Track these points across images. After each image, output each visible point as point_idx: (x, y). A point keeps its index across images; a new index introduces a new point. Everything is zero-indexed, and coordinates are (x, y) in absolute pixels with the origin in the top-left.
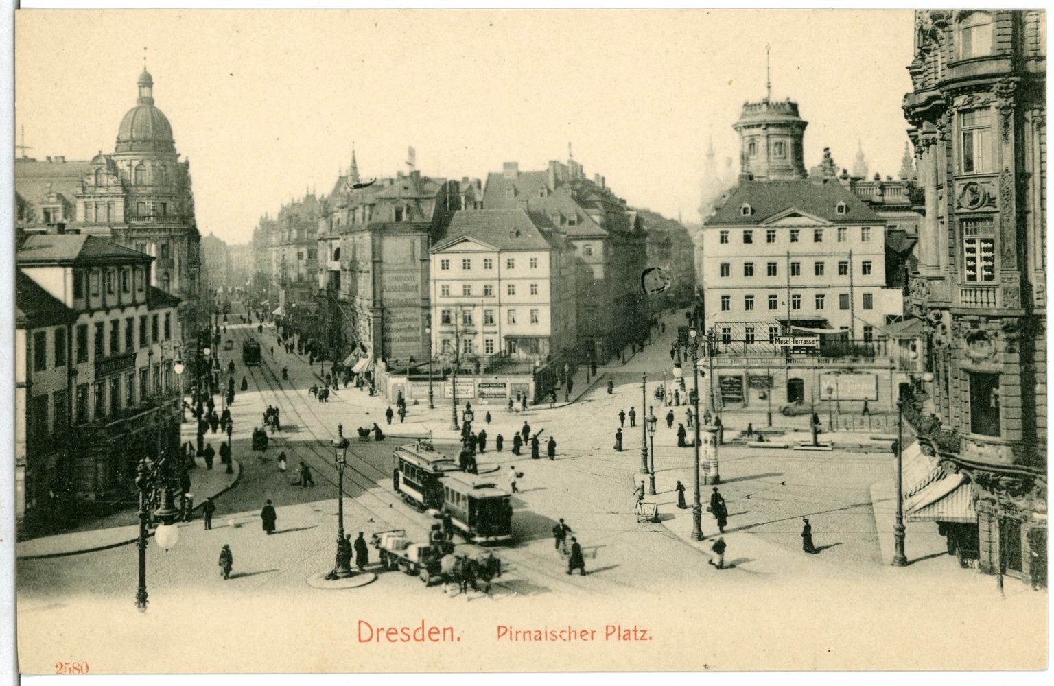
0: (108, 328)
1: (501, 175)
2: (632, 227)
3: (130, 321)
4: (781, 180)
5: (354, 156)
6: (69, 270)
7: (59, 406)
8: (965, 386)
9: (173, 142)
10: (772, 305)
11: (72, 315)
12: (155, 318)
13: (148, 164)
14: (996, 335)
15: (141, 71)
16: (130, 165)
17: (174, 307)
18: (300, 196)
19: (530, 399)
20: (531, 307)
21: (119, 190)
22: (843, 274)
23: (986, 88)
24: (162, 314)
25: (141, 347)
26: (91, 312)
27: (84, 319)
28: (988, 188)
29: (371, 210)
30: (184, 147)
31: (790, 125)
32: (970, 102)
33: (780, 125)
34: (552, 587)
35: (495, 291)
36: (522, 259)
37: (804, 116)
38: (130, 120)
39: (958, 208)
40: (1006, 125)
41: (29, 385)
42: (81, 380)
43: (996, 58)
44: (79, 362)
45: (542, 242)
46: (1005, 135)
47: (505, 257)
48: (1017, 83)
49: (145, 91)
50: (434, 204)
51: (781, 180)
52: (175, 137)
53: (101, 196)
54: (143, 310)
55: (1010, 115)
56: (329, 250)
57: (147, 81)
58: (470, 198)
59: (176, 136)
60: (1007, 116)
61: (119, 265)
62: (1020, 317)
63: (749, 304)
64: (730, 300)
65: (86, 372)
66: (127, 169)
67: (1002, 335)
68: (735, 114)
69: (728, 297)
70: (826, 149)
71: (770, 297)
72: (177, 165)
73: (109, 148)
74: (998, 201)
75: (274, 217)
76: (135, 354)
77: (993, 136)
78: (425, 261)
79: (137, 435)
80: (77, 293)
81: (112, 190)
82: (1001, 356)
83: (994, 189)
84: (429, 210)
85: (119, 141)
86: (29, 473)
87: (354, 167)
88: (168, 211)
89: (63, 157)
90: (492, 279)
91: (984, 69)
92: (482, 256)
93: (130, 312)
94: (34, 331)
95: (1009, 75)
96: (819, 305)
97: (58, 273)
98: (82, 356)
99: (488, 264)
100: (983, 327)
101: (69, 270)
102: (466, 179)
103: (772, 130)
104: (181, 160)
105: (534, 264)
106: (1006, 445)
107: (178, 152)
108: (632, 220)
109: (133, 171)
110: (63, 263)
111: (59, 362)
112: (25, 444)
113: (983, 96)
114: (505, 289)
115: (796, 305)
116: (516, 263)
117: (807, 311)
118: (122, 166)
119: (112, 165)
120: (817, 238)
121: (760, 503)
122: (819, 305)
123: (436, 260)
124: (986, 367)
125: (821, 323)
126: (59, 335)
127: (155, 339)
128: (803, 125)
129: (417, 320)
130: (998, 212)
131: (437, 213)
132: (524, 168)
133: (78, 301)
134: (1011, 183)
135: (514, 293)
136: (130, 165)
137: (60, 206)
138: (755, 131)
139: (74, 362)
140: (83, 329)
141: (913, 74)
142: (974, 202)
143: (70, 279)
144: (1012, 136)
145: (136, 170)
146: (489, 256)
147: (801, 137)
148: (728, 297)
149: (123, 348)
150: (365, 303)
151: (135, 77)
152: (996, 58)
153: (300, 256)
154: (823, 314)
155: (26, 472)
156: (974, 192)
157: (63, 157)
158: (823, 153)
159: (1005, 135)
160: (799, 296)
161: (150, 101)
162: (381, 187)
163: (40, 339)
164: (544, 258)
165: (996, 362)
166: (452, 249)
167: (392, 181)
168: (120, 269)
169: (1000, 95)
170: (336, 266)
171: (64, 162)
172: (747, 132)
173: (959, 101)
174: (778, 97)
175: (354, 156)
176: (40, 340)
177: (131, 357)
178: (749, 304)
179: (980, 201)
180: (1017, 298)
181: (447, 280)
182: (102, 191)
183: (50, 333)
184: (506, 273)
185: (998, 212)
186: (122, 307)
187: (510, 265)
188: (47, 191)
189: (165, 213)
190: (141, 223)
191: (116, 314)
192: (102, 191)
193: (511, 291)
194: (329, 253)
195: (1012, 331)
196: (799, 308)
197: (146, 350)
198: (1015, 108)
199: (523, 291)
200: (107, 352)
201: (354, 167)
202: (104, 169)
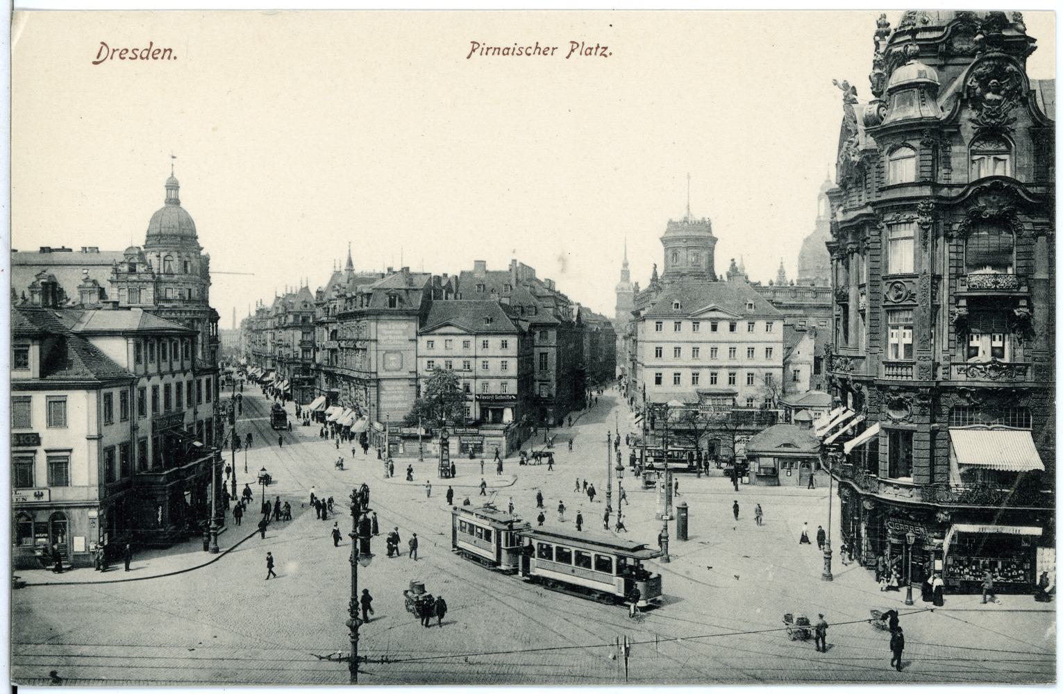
1: (470, 274)
2: (575, 319)
7: (124, 457)
8: (885, 441)
9: (196, 238)
10: (695, 379)
11: (132, 382)
12: (199, 382)
14: (912, 401)
16: (159, 256)
17: (213, 374)
19: (503, 453)
25: (189, 407)
27: (143, 382)
29: (368, 299)
30: (207, 242)
36: (495, 341)
37: (715, 234)
39: (885, 302)
40: (926, 237)
46: (925, 244)
48: (935, 204)
50: (421, 295)
51: (691, 279)
55: (929, 229)
56: (326, 333)
57: (173, 186)
58: (449, 290)
60: (927, 230)
63: (677, 380)
64: (681, 376)
69: (679, 374)
70: (733, 260)
71: (675, 374)
72: (200, 257)
73: (140, 241)
74: (917, 297)
79: (190, 482)
87: (350, 263)
88: (192, 295)
89: (97, 248)
91: (909, 193)
96: (732, 381)
98: (142, 412)
102: (445, 275)
105: (504, 345)
106: (917, 487)
107: (201, 245)
108: (575, 313)
109: (162, 261)
110: (125, 334)
111: (124, 418)
112: (97, 488)
115: (714, 381)
117: (723, 384)
120: (732, 328)
122: (732, 381)
124: (903, 425)
125: (732, 395)
127: (199, 400)
128: (715, 240)
130: (917, 305)
132: (491, 267)
136: (159, 256)
138: (677, 244)
140: (143, 390)
143: (131, 347)
144: (929, 245)
145: (165, 260)
147: (713, 249)
148: (679, 374)
151: (163, 180)
154: (735, 388)
155: (98, 512)
157: (97, 248)
158: (731, 262)
159: (925, 244)
161: (177, 202)
162: (374, 280)
163: (108, 398)
165: (911, 422)
166: (437, 331)
167: (383, 276)
168: (171, 341)
169: (921, 213)
171: (98, 252)
173: (888, 218)
178: (677, 380)
179: (903, 296)
182: (134, 278)
183: (116, 393)
187: (485, 345)
188: (85, 277)
191: (169, 379)
195: (925, 399)
196: (715, 383)
198: (933, 224)
200: (162, 410)
201: (350, 263)
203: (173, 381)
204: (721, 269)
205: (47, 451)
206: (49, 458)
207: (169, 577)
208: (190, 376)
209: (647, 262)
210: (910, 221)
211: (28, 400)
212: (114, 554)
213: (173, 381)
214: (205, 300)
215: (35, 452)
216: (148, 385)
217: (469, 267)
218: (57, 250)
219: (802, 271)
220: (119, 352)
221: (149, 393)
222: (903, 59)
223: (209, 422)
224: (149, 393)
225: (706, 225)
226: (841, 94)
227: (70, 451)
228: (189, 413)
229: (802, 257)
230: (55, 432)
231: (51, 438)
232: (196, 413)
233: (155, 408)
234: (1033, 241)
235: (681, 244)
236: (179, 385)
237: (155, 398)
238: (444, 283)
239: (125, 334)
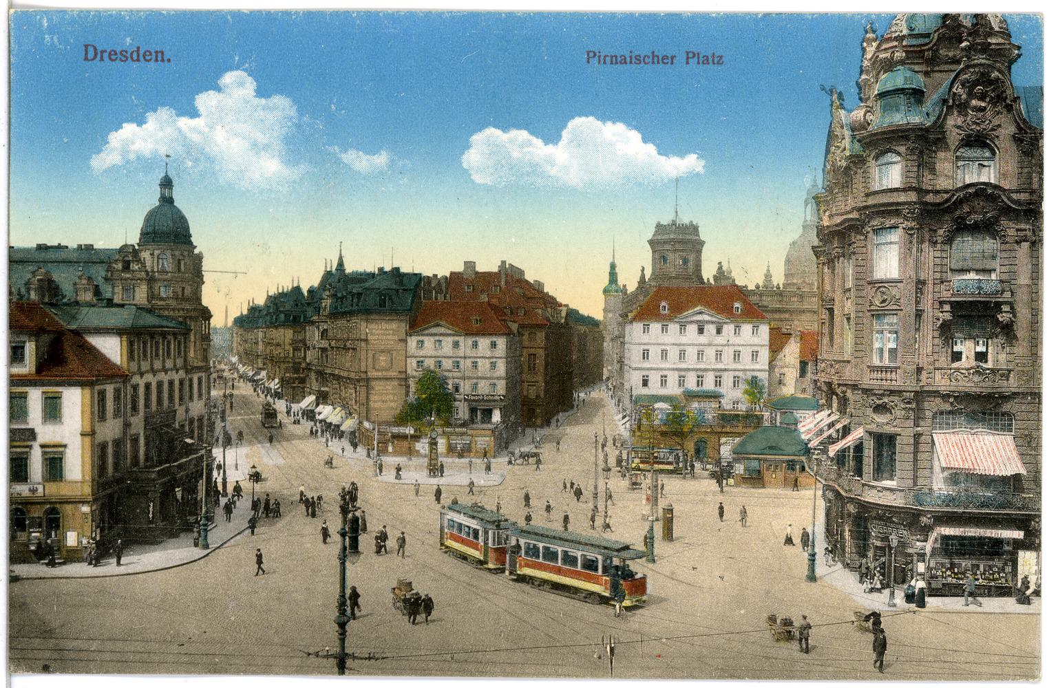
0: (166, 387)
3: (171, 383)
5: (341, 254)
9: (190, 236)
12: (191, 380)
15: (163, 175)
18: (287, 285)
22: (729, 357)
25: (180, 405)
36: (484, 342)
38: (151, 217)
42: (133, 431)
43: (904, 190)
44: (132, 415)
52: (192, 231)
54: (182, 373)
59: (193, 230)
61: (164, 335)
62: (916, 392)
76: (175, 411)
80: (131, 356)
86: (94, 508)
88: (186, 294)
90: (461, 357)
92: (450, 339)
93: (162, 376)
94: (97, 388)
95: (915, 203)
99: (456, 345)
102: (435, 276)
104: (196, 251)
105: (494, 345)
108: (564, 314)
109: (156, 259)
117: (709, 385)
120: (719, 331)
121: (153, 489)
124: (889, 429)
125: (715, 396)
126: (117, 391)
127: (191, 398)
129: (881, 361)
130: (901, 310)
133: (132, 364)
139: (129, 415)
140: (135, 387)
145: (158, 258)
146: (456, 338)
152: (904, 190)
160: (666, 377)
163: (102, 394)
164: (501, 342)
166: (426, 332)
173: (876, 222)
175: (341, 254)
181: (422, 357)
183: (110, 389)
185: (901, 310)
186: (154, 372)
189: (183, 295)
190: (162, 303)
194: (317, 334)
197: (184, 408)
198: (918, 229)
199: (484, 366)
204: (708, 273)
205: (42, 446)
206: (44, 453)
214: (197, 298)
216: (141, 382)
217: (460, 268)
221: (141, 391)
224: (141, 391)
232: (187, 411)
233: (147, 406)
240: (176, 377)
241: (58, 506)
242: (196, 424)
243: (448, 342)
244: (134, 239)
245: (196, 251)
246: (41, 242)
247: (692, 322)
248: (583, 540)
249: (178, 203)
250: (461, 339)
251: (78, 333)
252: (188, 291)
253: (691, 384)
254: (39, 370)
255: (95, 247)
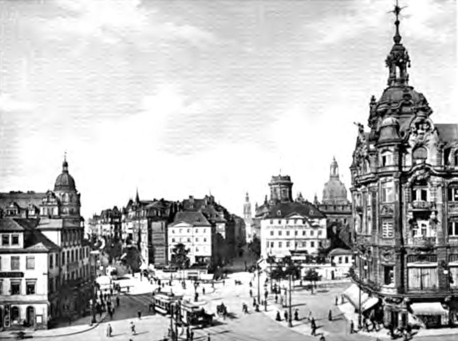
3: (77, 251)
4: (284, 204)
6: (59, 232)
10: (288, 245)
12: (84, 249)
13: (67, 195)
15: (64, 161)
20: (288, 241)
21: (56, 204)
23: (391, 175)
24: (85, 248)
26: (66, 247)
27: (65, 250)
28: (391, 207)
31: (287, 183)
32: (386, 180)
33: (283, 184)
34: (350, 322)
35: (191, 240)
36: (201, 229)
38: (59, 179)
41: (49, 274)
45: (208, 223)
47: (195, 228)
49: (65, 168)
51: (284, 204)
53: (50, 206)
57: (66, 165)
65: (64, 268)
66: (59, 196)
67: (395, 254)
68: (269, 180)
73: (52, 188)
75: (99, 214)
77: (392, 192)
78: (167, 230)
81: (54, 204)
82: (395, 260)
83: (393, 207)
84: (168, 212)
85: (56, 186)
93: (74, 249)
94: (50, 254)
97: (55, 233)
100: (389, 251)
101: (59, 232)
103: (282, 186)
110: (57, 230)
113: (389, 178)
114: (195, 240)
116: (199, 231)
118: (57, 194)
119: (53, 194)
123: (170, 229)
125: (305, 252)
127: (84, 257)
131: (167, 212)
134: (398, 206)
135: (198, 241)
137: (17, 209)
138: (276, 186)
140: (64, 253)
141: (351, 170)
142: (386, 211)
149: (75, 260)
150: (144, 244)
153: (112, 228)
156: (386, 208)
159: (397, 191)
161: (67, 172)
163: (51, 258)
169: (395, 178)
170: (131, 231)
172: (273, 186)
173: (382, 179)
174: (283, 174)
176: (51, 258)
177: (77, 263)
180: (400, 242)
184: (195, 234)
192: (50, 204)
193: (197, 240)
199: (201, 240)
202: (51, 196)
203: (70, 250)
204: (295, 197)
205: (26, 279)
206: (27, 283)
207: (87, 332)
208: (80, 247)
209: (261, 193)
210: (390, 181)
211: (18, 258)
212: (51, 325)
213: (70, 250)
214: (78, 212)
215: (21, 280)
216: (65, 250)
217: (187, 198)
218: (16, 193)
219: (324, 197)
220: (55, 237)
221: (66, 255)
222: (383, 114)
223: (87, 266)
224: (66, 255)
225: (289, 178)
226: (357, 128)
227: (36, 279)
228: (80, 262)
229: (324, 192)
230: (29, 271)
231: (28, 274)
232: (83, 262)
233: (68, 261)
234: (436, 188)
235: (278, 186)
236: (77, 251)
237: (68, 256)
238: (178, 204)
239: (57, 230)
240: (78, 248)
241: (34, 305)
242: (86, 268)
243: (185, 230)
244: (52, 188)
245: (78, 193)
246: (12, 190)
247: (292, 219)
248: (11, 251)
249: (70, 173)
250: (191, 228)
251: (40, 230)
252: (75, 210)
253: (292, 248)
254: (25, 246)
255: (125, 207)
